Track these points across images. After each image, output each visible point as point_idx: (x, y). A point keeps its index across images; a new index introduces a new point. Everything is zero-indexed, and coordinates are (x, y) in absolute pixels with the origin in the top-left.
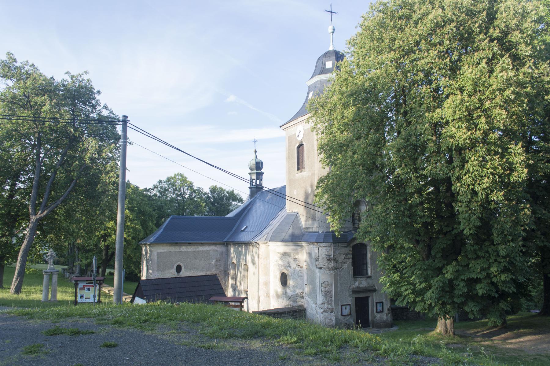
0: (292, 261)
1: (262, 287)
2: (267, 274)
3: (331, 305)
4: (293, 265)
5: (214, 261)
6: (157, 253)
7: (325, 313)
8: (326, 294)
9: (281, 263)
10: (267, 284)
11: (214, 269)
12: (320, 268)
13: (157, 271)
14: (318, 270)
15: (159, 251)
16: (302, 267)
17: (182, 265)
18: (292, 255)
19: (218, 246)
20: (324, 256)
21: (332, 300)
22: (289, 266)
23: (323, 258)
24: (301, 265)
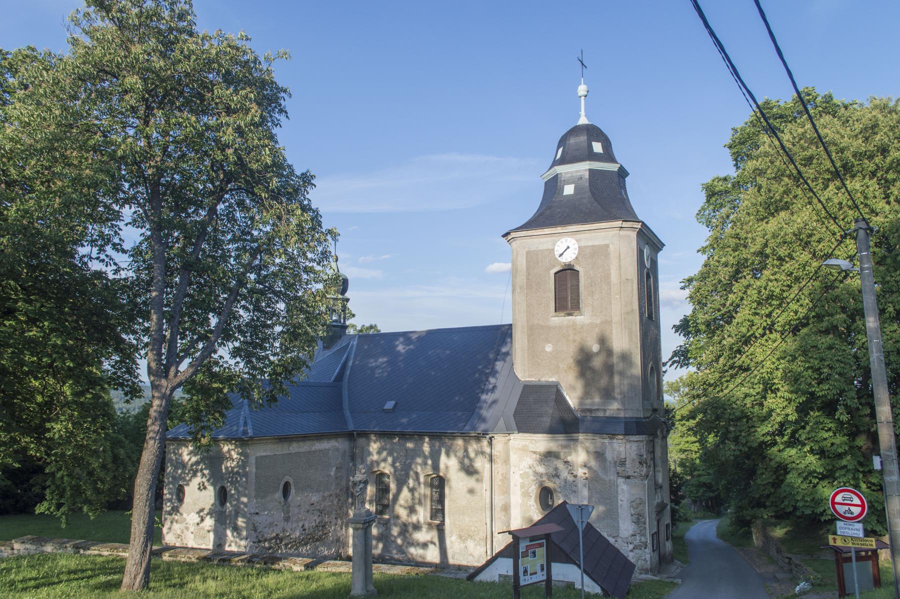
0: (560, 465)
1: (498, 514)
2: (507, 491)
3: (645, 535)
4: (564, 474)
5: (334, 469)
6: (257, 458)
7: (637, 551)
8: (638, 519)
9: (541, 469)
10: (506, 508)
11: (333, 487)
12: (628, 477)
13: (256, 497)
14: (621, 481)
15: (259, 454)
16: (575, 476)
17: (291, 481)
18: (562, 455)
19: (339, 440)
20: (635, 457)
21: (645, 528)
22: (557, 476)
23: (633, 460)
24: (575, 473)
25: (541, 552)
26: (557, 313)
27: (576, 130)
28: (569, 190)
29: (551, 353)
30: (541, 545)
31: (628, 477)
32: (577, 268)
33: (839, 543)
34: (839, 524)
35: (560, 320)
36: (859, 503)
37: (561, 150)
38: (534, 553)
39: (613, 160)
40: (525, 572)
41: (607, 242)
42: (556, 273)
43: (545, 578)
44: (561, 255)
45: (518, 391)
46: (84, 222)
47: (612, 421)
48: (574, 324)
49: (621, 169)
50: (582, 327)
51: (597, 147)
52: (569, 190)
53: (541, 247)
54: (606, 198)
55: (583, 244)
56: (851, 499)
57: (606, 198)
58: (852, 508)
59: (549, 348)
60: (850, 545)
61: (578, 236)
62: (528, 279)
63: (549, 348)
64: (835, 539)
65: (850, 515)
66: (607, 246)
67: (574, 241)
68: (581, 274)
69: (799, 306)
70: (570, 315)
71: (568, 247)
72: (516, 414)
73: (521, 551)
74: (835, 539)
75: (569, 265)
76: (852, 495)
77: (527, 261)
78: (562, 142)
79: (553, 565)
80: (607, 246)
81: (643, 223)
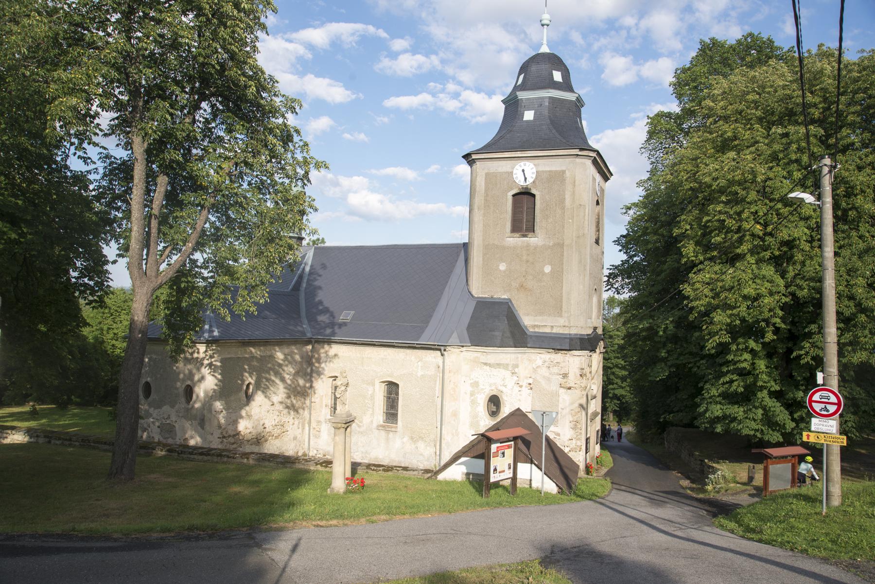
12: (569, 388)
14: (562, 391)
25: (510, 453)
26: (513, 234)
27: (538, 58)
28: (529, 115)
29: (504, 272)
30: (509, 447)
31: (569, 388)
32: (533, 191)
33: (812, 439)
34: (814, 421)
35: (515, 241)
36: (836, 401)
37: (522, 77)
38: (503, 453)
39: (570, 89)
40: (495, 470)
41: (564, 168)
42: (513, 196)
43: (511, 475)
45: (471, 307)
46: (16, 136)
48: (528, 245)
49: (579, 99)
50: (535, 248)
51: (557, 76)
52: (529, 115)
53: (500, 170)
54: (563, 130)
55: (541, 169)
56: (828, 398)
57: (563, 130)
58: (828, 406)
59: (503, 267)
60: (822, 442)
61: (537, 161)
62: (486, 200)
63: (503, 267)
64: (808, 436)
65: (825, 413)
66: (564, 172)
67: (532, 165)
68: (537, 198)
70: (525, 236)
71: (523, 171)
72: (469, 328)
73: (492, 451)
74: (808, 436)
75: (527, 188)
76: (830, 394)
77: (486, 183)
78: (524, 68)
79: (519, 464)
80: (564, 172)
81: (598, 152)
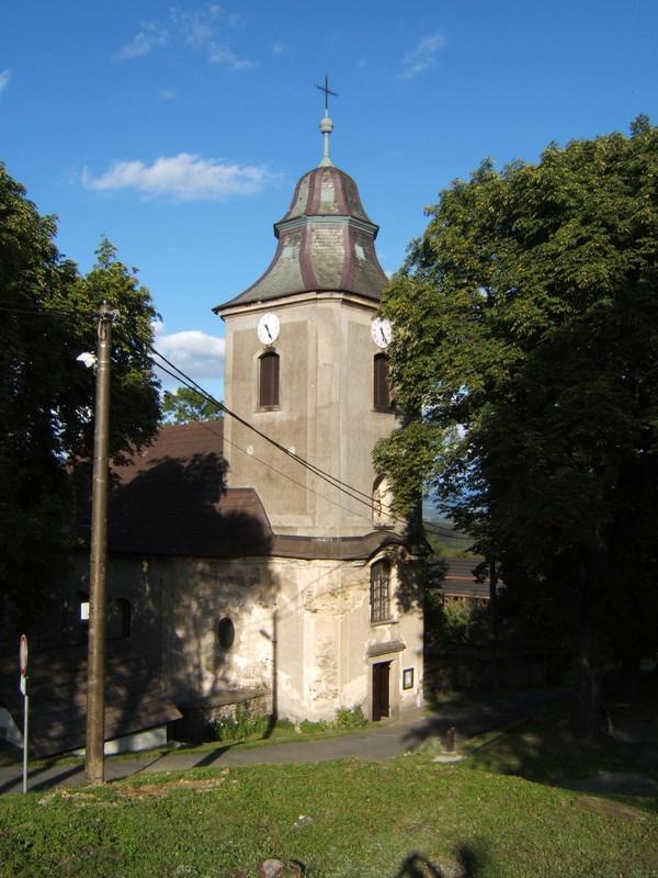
8: (325, 662)
21: (335, 673)
31: (315, 611)
32: (277, 352)
41: (306, 318)
44: (270, 336)
47: (418, 511)
55: (284, 322)
61: (282, 311)
66: (306, 322)
68: (281, 359)
69: (247, 470)
70: (270, 410)
71: (266, 326)
80: (306, 322)
